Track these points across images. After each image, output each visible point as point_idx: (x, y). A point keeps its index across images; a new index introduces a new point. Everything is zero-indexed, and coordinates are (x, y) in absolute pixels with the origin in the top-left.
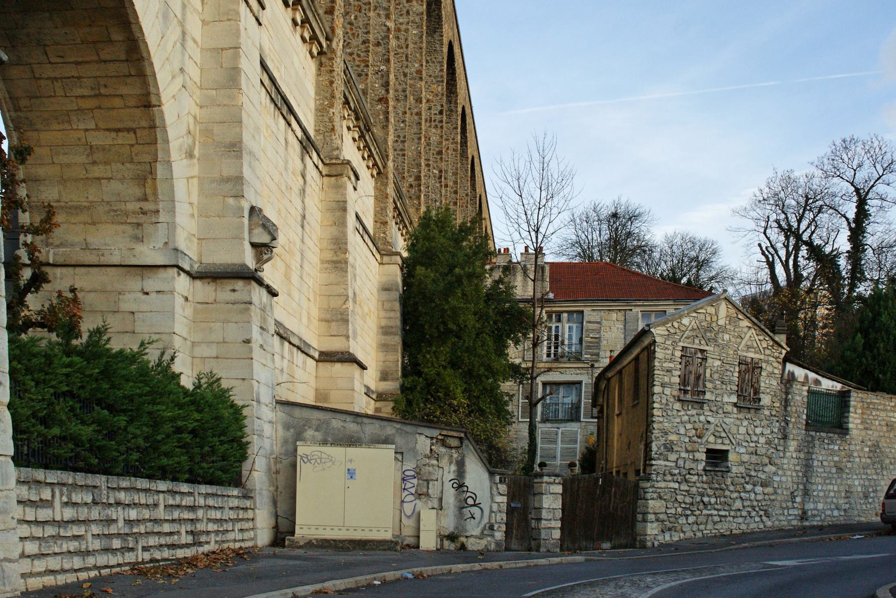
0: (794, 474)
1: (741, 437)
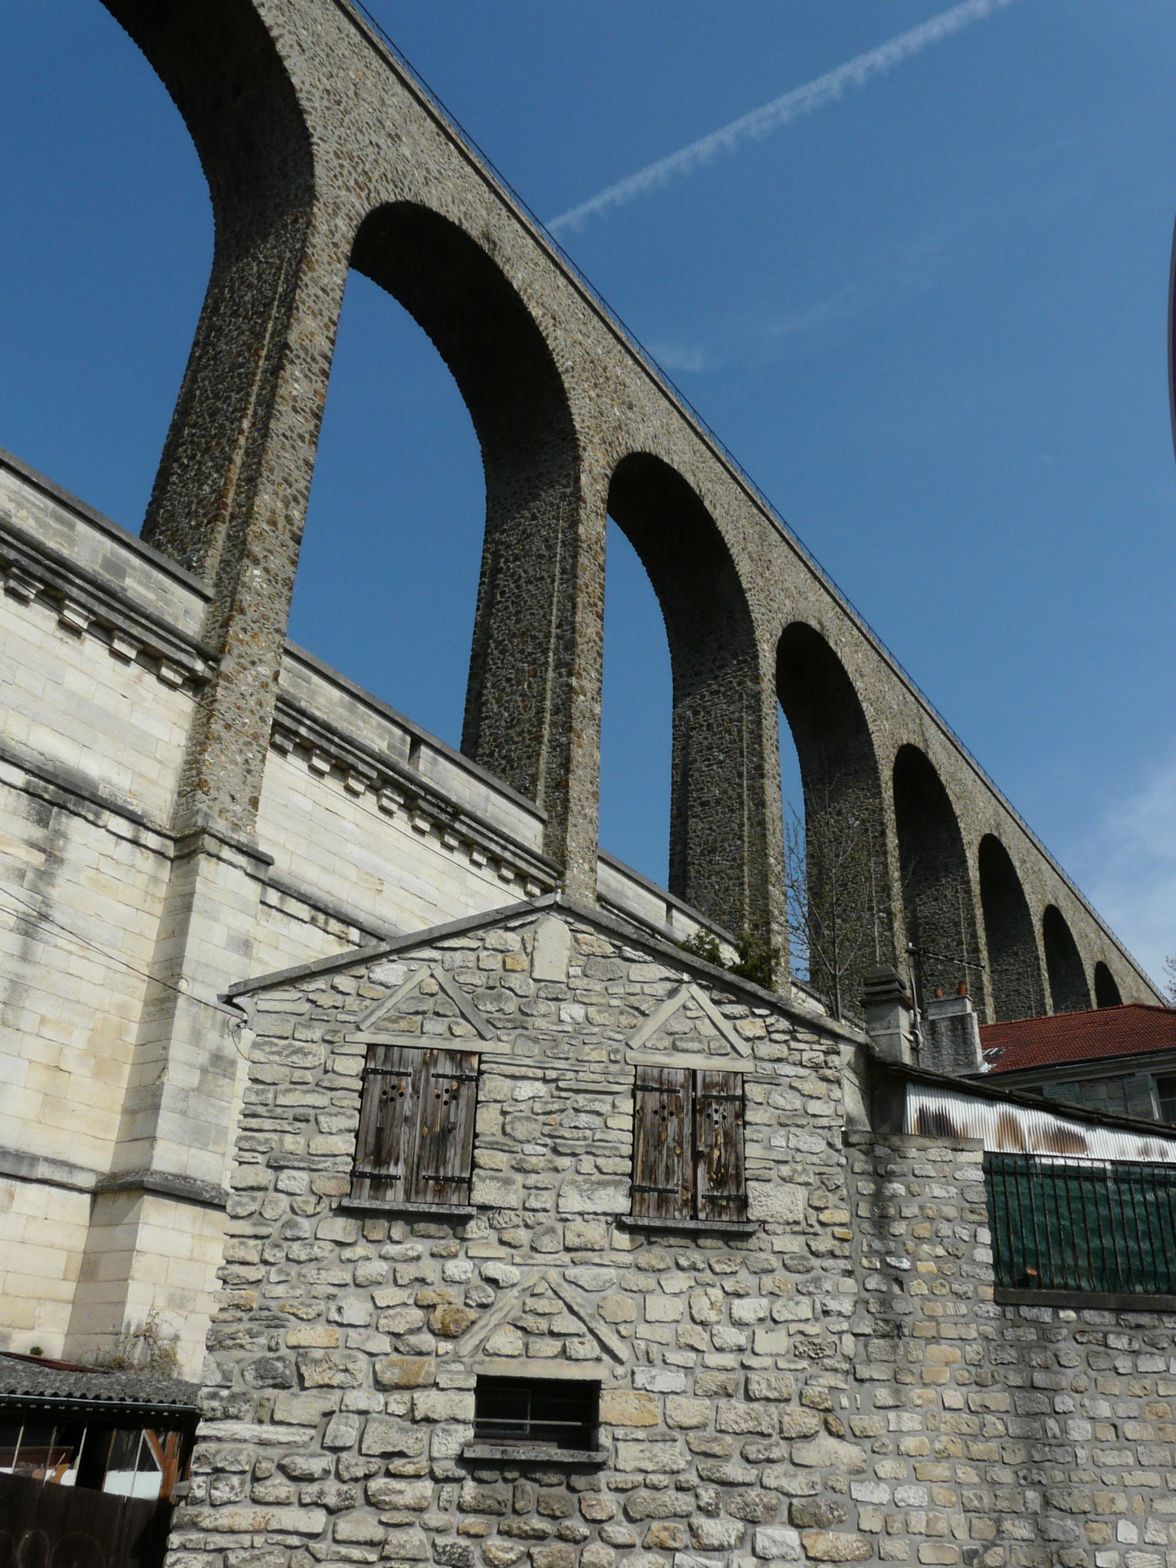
0: (967, 1474)
1: (664, 1334)
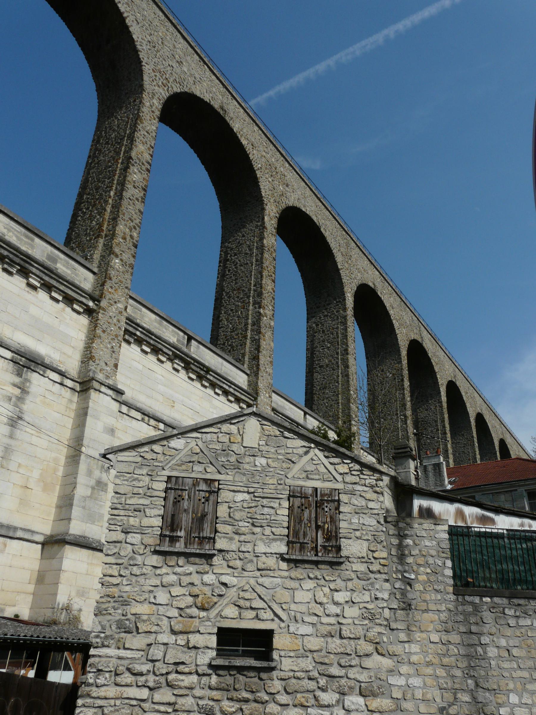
0: (441, 672)
1: (303, 608)
